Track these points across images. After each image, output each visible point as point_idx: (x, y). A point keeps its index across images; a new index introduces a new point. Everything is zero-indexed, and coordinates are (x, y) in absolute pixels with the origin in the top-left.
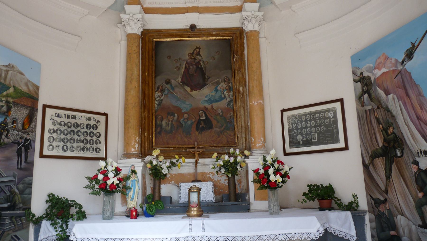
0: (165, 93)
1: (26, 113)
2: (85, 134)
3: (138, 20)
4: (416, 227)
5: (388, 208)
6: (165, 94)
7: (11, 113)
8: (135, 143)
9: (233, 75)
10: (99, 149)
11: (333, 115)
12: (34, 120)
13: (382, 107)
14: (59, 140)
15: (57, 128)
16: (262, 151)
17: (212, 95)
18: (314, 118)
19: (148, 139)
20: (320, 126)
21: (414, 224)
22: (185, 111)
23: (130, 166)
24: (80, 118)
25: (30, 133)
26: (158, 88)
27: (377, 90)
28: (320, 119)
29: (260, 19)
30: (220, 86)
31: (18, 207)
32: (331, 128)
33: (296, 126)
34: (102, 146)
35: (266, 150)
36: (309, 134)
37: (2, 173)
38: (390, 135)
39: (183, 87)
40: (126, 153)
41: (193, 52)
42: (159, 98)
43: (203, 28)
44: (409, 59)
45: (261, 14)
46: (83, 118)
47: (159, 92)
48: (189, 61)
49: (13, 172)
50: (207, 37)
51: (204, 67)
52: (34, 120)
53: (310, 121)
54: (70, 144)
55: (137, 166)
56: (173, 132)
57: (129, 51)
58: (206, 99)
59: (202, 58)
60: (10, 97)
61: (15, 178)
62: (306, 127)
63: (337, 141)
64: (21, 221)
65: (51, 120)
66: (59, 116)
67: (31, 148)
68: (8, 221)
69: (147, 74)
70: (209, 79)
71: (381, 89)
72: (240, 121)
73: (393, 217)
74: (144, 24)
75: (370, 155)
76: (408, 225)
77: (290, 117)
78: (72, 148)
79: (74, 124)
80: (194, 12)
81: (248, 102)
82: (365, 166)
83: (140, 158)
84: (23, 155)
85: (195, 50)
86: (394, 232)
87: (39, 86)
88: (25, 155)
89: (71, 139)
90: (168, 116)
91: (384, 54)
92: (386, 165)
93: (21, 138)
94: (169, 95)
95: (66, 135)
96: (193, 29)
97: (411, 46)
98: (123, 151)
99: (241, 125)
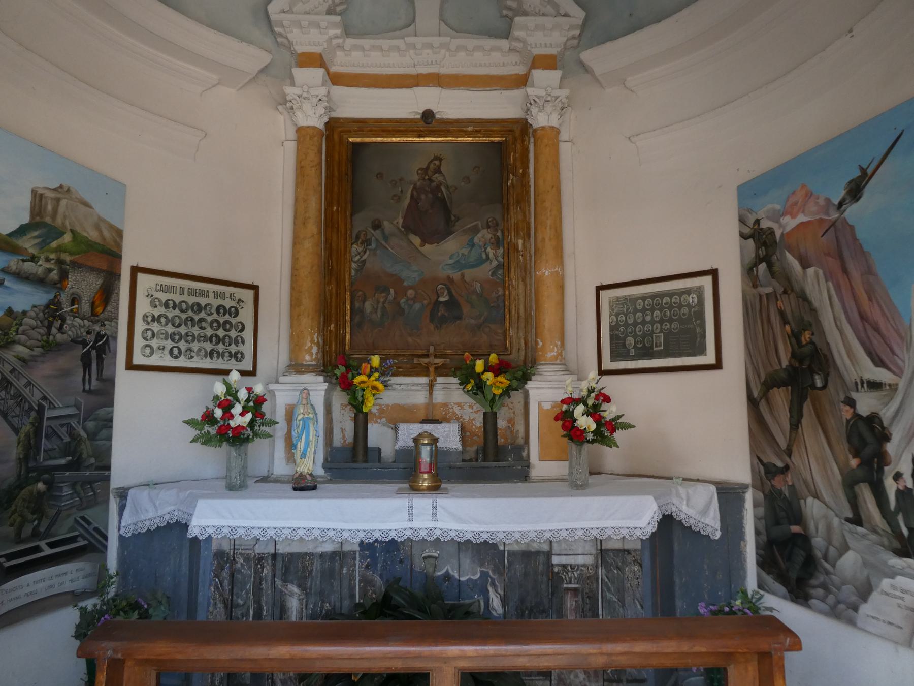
0: (370, 247)
1: (98, 283)
2: (215, 325)
3: (318, 98)
4: (841, 522)
5: (790, 483)
6: (370, 250)
7: (68, 284)
9: (506, 215)
10: (242, 353)
11: (696, 300)
12: (114, 296)
13: (792, 290)
14: (163, 336)
15: (160, 313)
17: (463, 254)
18: (659, 304)
20: (671, 321)
21: (837, 515)
22: (410, 284)
23: (302, 388)
24: (205, 294)
25: (106, 322)
26: (358, 237)
27: (785, 256)
28: (671, 307)
29: (563, 103)
30: (480, 235)
31: (87, 464)
32: (692, 326)
34: (247, 349)
35: (565, 365)
36: (649, 335)
37: (55, 401)
38: (803, 346)
40: (293, 363)
41: (428, 168)
42: (358, 257)
44: (852, 200)
45: (564, 93)
46: (211, 295)
47: (359, 245)
48: (418, 184)
49: (76, 399)
50: (455, 137)
52: (113, 296)
53: (652, 310)
54: (185, 344)
55: (313, 390)
59: (445, 179)
60: (65, 252)
61: (79, 408)
62: (644, 323)
63: (702, 351)
64: (93, 490)
65: (147, 296)
67: (110, 351)
68: (67, 491)
69: (335, 208)
70: (457, 221)
71: (793, 256)
73: (799, 500)
74: (330, 108)
75: (762, 381)
76: (825, 517)
79: (193, 305)
81: (533, 270)
82: (752, 402)
83: (321, 373)
84: (94, 365)
85: (431, 161)
86: (798, 527)
87: (122, 229)
88: (98, 365)
89: (187, 335)
90: (375, 294)
91: (803, 186)
92: (791, 401)
93: (88, 333)
94: (378, 252)
97: (857, 173)
99: (518, 313)
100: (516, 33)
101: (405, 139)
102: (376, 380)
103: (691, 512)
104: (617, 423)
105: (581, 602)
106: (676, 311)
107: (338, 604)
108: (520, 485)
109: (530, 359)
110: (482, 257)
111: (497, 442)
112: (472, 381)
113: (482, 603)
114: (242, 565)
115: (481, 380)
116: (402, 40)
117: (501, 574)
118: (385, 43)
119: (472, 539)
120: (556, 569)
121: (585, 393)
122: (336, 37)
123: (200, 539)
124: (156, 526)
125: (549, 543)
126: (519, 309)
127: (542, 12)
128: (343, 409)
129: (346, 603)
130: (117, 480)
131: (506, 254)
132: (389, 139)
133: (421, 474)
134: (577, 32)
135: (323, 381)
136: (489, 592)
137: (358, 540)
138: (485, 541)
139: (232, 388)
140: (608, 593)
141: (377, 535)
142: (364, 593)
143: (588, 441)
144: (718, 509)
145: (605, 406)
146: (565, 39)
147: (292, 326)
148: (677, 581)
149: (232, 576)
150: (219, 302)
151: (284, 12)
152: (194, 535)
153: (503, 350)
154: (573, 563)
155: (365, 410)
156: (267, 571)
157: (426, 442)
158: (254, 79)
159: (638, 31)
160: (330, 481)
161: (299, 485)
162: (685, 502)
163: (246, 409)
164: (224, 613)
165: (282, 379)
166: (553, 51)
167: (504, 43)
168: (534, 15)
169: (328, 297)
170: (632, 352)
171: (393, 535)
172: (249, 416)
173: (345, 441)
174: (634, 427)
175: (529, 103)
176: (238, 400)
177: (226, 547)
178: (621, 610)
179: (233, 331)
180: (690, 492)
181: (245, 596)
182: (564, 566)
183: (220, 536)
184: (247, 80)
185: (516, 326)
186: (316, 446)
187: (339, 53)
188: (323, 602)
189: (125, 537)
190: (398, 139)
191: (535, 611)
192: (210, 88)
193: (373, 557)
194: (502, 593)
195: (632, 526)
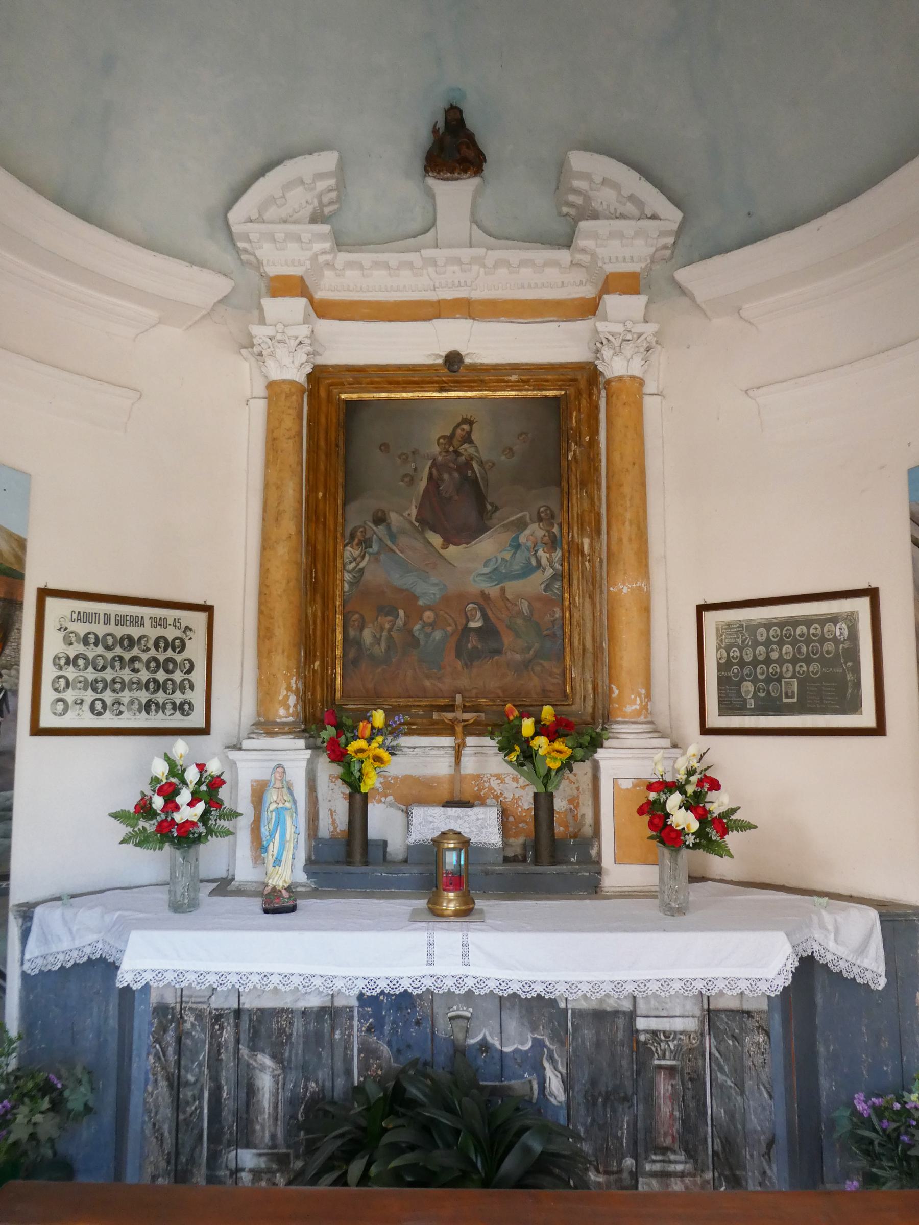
0: (370, 550)
2: (153, 664)
3: (298, 341)
6: (370, 554)
8: (287, 692)
9: (565, 503)
10: (190, 704)
11: (846, 632)
12: (14, 634)
14: (82, 685)
16: (640, 726)
17: (503, 559)
18: (790, 635)
19: (323, 678)
20: (808, 660)
24: (138, 621)
26: (353, 536)
28: (808, 642)
30: (527, 532)
32: (839, 670)
33: (739, 655)
34: (197, 697)
35: (652, 723)
39: (422, 532)
40: (262, 720)
41: (453, 434)
42: (353, 565)
43: (482, 364)
45: (650, 329)
46: (147, 622)
48: (440, 458)
51: (483, 478)
52: (13, 634)
53: (781, 643)
56: (394, 660)
57: (273, 432)
58: (487, 570)
59: (477, 451)
62: (768, 661)
63: (855, 707)
65: (59, 630)
66: (84, 618)
67: (9, 712)
69: (320, 495)
70: (495, 511)
72: (579, 635)
77: (722, 629)
78: (116, 706)
79: (122, 639)
80: (458, 316)
81: (605, 582)
83: (302, 734)
85: (458, 425)
89: (114, 681)
94: (382, 557)
95: (101, 671)
96: (453, 366)
98: (256, 712)
99: (584, 645)
100: (581, 242)
101: (421, 394)
102: (380, 747)
103: (841, 951)
104: (730, 820)
105: (679, 1086)
106: (817, 647)
107: (328, 1084)
108: (589, 905)
109: (601, 712)
110: (530, 563)
111: (553, 835)
112: (517, 748)
113: (535, 1086)
114: (193, 1025)
115: (530, 747)
116: (418, 253)
117: (562, 1043)
118: (393, 258)
119: (520, 992)
120: (642, 1038)
121: (682, 777)
122: (324, 252)
123: (134, 988)
124: (73, 963)
125: (631, 999)
126: (584, 639)
127: (618, 212)
128: (332, 782)
129: (340, 1082)
130: (18, 894)
131: (566, 559)
132: (398, 395)
133: (445, 893)
134: (671, 240)
135: (304, 747)
136: (544, 1069)
137: (357, 992)
138: (539, 995)
139: (176, 766)
140: (719, 1075)
141: (383, 985)
142: (365, 1066)
143: (688, 847)
144: (881, 945)
145: (711, 795)
146: (653, 250)
147: (260, 667)
148: (821, 1049)
149: (179, 1040)
150: (159, 632)
151: (251, 221)
152: (126, 984)
153: (561, 698)
154: (668, 1029)
155: (364, 789)
156: (227, 1034)
157: (452, 846)
158: (208, 315)
159: (762, 241)
160: (315, 893)
161: (272, 906)
162: (832, 936)
163: (196, 796)
164: (168, 1094)
165: (246, 744)
166: (635, 267)
167: (564, 256)
168: (608, 218)
169: (311, 622)
170: (751, 704)
171: (405, 985)
172: (201, 807)
173: (335, 828)
174: (755, 827)
175: (599, 343)
176: (184, 782)
177: (170, 999)
178: (739, 1099)
179: (178, 672)
180: (839, 919)
181: (197, 1070)
182: (655, 1033)
183: (161, 985)
184: (199, 316)
185: (580, 664)
186: (295, 848)
187: (328, 273)
188: (307, 1080)
189: (29, 975)
190: (410, 395)
191: (612, 1098)
192: (146, 330)
193: (377, 1016)
194: (564, 1071)
195: (754, 976)
